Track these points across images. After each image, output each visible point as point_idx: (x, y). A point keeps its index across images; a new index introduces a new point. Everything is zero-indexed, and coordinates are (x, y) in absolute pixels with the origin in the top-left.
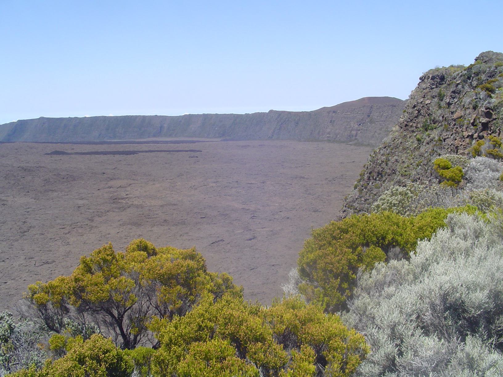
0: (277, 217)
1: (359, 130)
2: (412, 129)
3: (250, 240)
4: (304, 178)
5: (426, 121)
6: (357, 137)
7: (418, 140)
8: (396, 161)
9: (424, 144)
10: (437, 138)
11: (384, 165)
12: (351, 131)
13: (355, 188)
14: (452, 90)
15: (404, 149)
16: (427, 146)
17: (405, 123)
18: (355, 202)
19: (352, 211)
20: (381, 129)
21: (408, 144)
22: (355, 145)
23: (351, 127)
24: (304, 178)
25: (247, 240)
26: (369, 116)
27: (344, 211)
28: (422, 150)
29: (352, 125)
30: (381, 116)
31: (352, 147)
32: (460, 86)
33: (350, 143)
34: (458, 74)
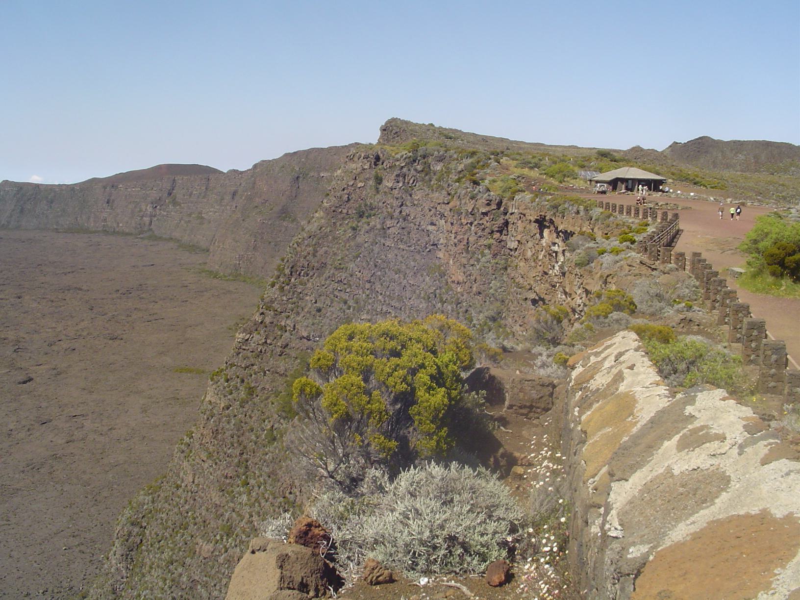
0: (55, 348)
1: (155, 216)
2: (342, 216)
3: (24, 382)
4: (80, 289)
5: (360, 206)
6: (152, 227)
7: (354, 229)
8: (326, 253)
9: (362, 233)
10: (379, 226)
11: (310, 257)
12: (142, 217)
13: (273, 285)
14: (395, 173)
15: (334, 238)
16: (367, 235)
17: (333, 208)
18: (273, 302)
19: (272, 313)
20: (190, 215)
21: (339, 232)
22: (150, 238)
23: (141, 211)
24: (80, 289)
25: (20, 383)
26: (170, 194)
27: (262, 313)
28: (359, 240)
29: (144, 208)
30: (190, 195)
31: (146, 242)
32: (405, 170)
33: (141, 236)
34: (402, 156)
